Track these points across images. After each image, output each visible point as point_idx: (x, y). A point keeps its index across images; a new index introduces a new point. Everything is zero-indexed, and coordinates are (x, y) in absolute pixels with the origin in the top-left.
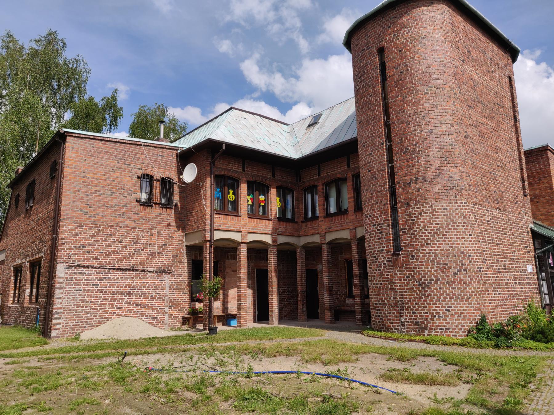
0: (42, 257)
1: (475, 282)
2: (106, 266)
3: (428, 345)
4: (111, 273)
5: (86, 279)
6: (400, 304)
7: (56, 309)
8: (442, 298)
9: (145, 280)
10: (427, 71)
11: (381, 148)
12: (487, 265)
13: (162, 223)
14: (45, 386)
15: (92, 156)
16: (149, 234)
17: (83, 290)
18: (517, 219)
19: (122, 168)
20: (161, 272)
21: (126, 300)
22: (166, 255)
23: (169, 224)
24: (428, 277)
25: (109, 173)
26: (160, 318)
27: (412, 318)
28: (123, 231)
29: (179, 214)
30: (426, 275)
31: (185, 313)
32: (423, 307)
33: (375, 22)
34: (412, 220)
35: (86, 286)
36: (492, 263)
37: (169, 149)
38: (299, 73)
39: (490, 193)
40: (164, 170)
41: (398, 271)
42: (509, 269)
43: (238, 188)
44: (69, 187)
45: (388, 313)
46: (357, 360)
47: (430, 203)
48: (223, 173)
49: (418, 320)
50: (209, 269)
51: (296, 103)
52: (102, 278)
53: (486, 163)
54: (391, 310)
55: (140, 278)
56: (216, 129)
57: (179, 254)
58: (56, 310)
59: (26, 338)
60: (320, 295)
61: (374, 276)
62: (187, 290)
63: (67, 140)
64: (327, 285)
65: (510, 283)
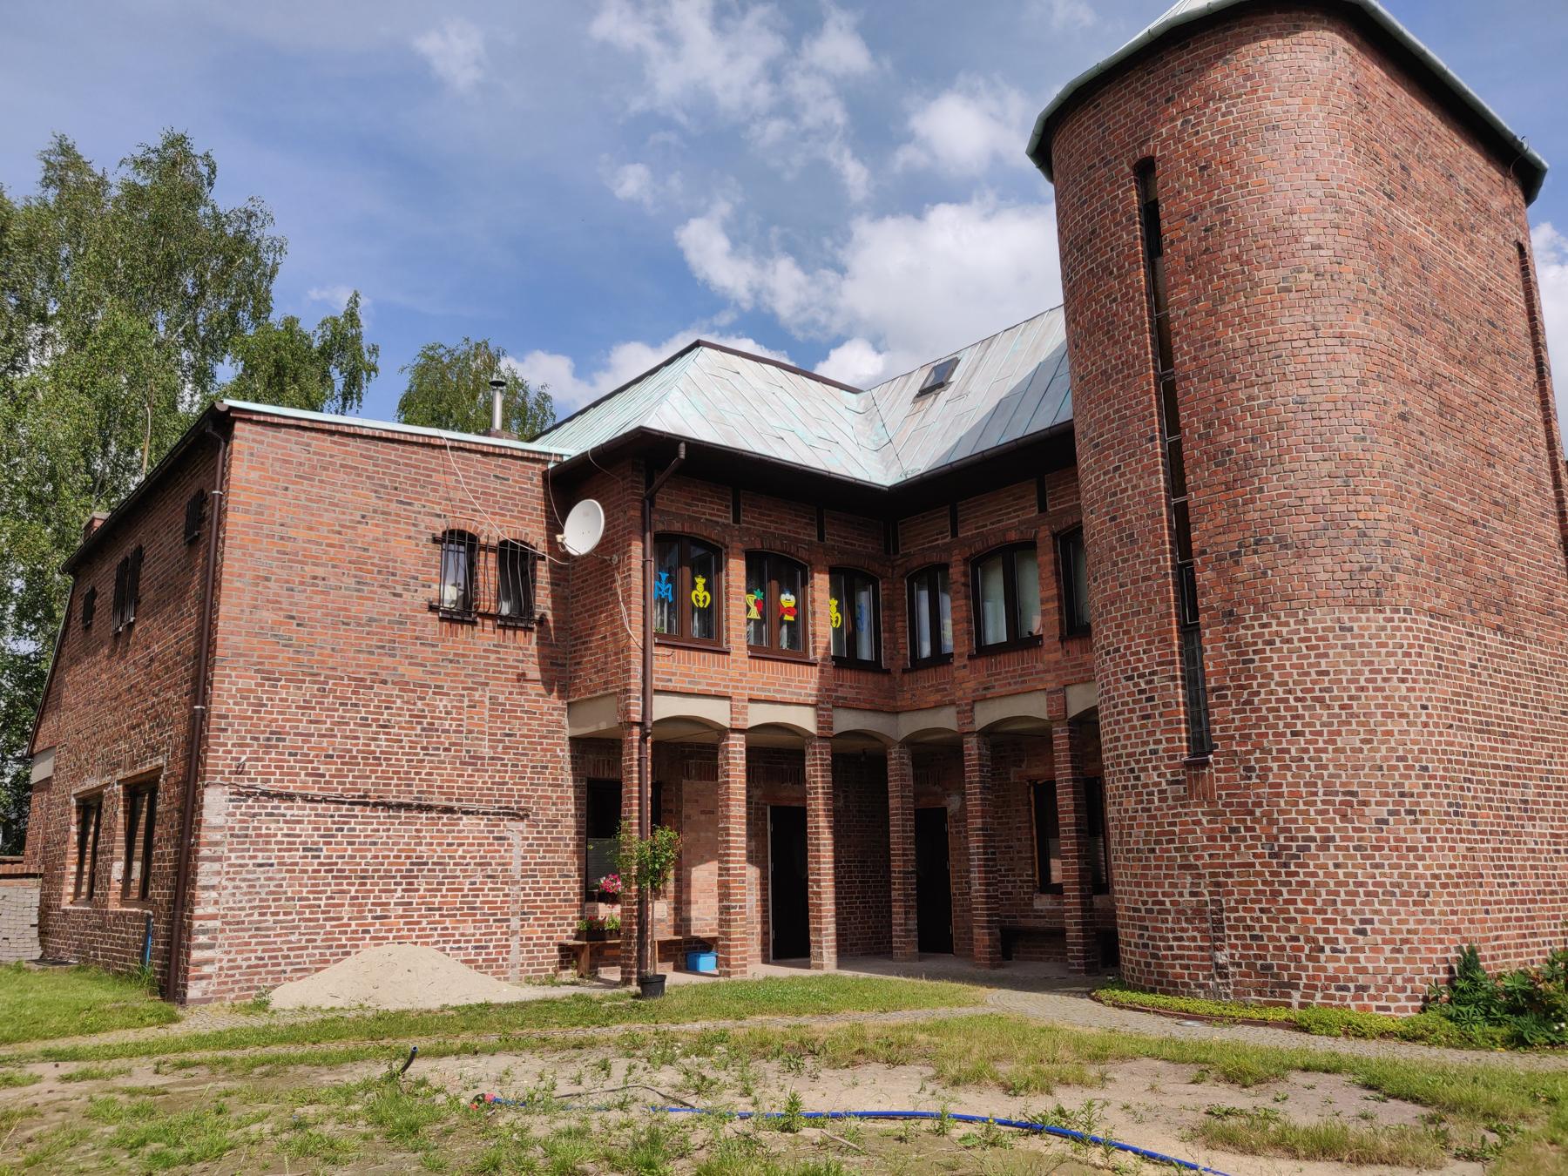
0: (160, 768)
1: (1441, 849)
2: (342, 796)
3: (1304, 1036)
4: (357, 817)
5: (285, 831)
6: (1213, 912)
7: (201, 918)
8: (1342, 894)
9: (454, 838)
10: (1286, 225)
11: (1147, 451)
12: (1474, 798)
13: (502, 673)
14: (186, 1150)
15: (305, 478)
16: (466, 703)
17: (279, 864)
18: (1555, 662)
19: (389, 514)
20: (499, 814)
21: (399, 894)
22: (513, 766)
23: (524, 674)
24: (1298, 830)
25: (354, 528)
26: (495, 947)
27: (1251, 952)
28: (391, 696)
29: (551, 645)
30: (1293, 826)
31: (566, 935)
32: (1285, 920)
33: (1126, 88)
34: (1245, 662)
35: (286, 854)
36: (1488, 791)
37: (522, 458)
38: (843, 256)
39: (1476, 583)
40: (508, 518)
41: (1203, 814)
42: (1538, 811)
43: (719, 569)
44: (242, 567)
45: (1176, 939)
46: (1103, 1078)
47: (1301, 613)
48: (677, 527)
49: (1269, 961)
50: (640, 805)
51: (838, 342)
52: (330, 829)
53: (1463, 496)
54: (1183, 930)
55: (438, 831)
56: (659, 402)
57: (549, 761)
58: (202, 922)
59: (117, 1001)
60: (956, 883)
61: (1131, 827)
62: (573, 868)
63: (236, 433)
64: (978, 854)
65: (1541, 852)
